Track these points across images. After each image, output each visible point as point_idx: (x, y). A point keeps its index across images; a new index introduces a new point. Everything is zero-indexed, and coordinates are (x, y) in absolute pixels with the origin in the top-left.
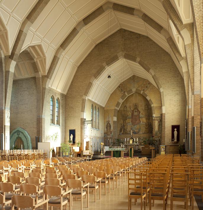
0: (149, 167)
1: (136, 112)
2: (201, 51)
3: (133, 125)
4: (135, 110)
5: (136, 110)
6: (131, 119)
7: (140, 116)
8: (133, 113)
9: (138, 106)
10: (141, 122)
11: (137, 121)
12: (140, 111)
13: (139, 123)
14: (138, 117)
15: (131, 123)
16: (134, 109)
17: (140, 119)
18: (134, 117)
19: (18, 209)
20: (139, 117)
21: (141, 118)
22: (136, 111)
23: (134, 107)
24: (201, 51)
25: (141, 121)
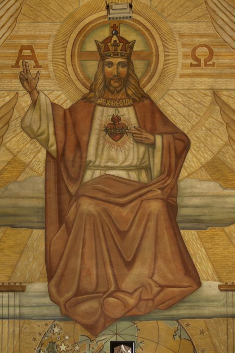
0: (193, 302)
1: (128, 142)
2: (190, 170)
3: (66, 317)
4: (103, 115)
5: (128, 115)
6: (39, 234)
7: (188, 204)
8: (80, 147)
9: (149, 57)
10: (210, 287)
11: (140, 271)
12: (183, 125)
13: (182, 299)
14: (155, 206)
15: (40, 287)
16: (88, 102)
17: (189, 236)
18: (87, 206)
19: (4, 298)
20: (171, 208)
21: (198, 223)
22: (115, 130)
23: (92, 67)
24: (190, 170)
25: (203, 266)
